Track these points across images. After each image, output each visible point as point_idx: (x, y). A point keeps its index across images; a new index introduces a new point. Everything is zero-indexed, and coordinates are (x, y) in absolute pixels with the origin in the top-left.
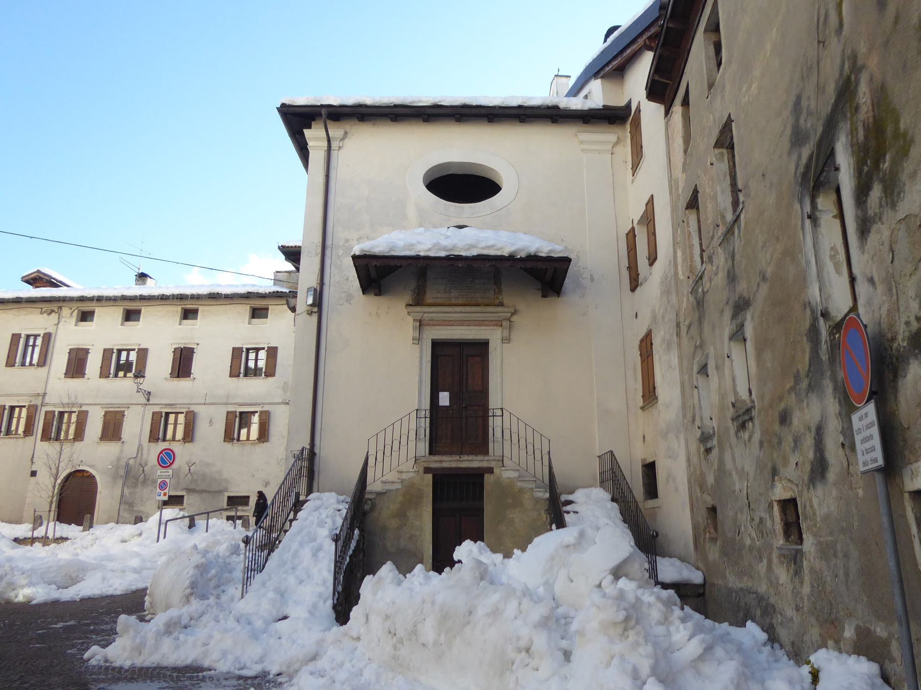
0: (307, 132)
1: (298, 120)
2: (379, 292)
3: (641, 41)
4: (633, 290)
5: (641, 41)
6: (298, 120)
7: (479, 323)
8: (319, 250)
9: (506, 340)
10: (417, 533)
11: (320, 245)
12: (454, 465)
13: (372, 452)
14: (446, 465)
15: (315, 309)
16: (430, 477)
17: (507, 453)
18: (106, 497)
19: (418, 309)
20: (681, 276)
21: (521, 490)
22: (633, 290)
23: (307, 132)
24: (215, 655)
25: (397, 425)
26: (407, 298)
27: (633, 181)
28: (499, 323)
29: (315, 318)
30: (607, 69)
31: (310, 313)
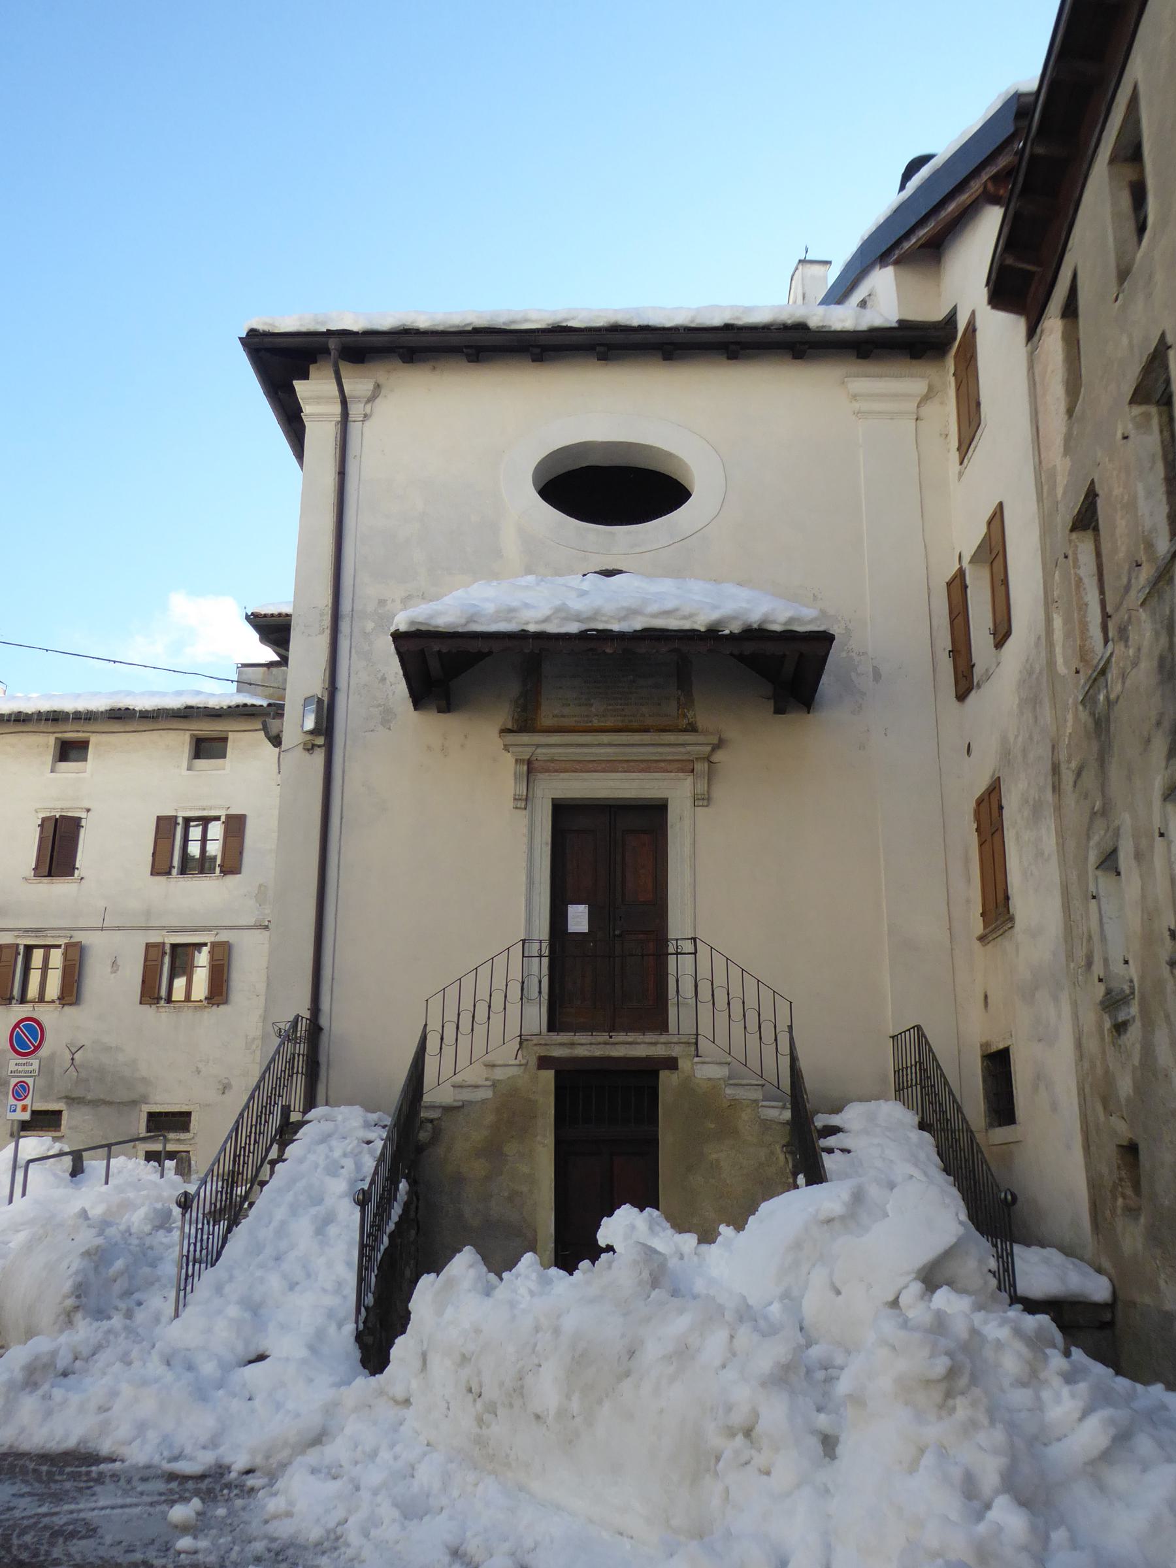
1: (281, 360)
2: (447, 705)
3: (976, 186)
5: (976, 186)
6: (281, 360)
7: (647, 766)
8: (327, 621)
9: (702, 800)
12: (598, 1052)
13: (434, 1026)
14: (581, 1052)
15: (320, 740)
16: (549, 1075)
18: (379, 676)
19: (525, 738)
23: (301, 388)
26: (504, 716)
28: (687, 767)
29: (319, 757)
31: (310, 748)
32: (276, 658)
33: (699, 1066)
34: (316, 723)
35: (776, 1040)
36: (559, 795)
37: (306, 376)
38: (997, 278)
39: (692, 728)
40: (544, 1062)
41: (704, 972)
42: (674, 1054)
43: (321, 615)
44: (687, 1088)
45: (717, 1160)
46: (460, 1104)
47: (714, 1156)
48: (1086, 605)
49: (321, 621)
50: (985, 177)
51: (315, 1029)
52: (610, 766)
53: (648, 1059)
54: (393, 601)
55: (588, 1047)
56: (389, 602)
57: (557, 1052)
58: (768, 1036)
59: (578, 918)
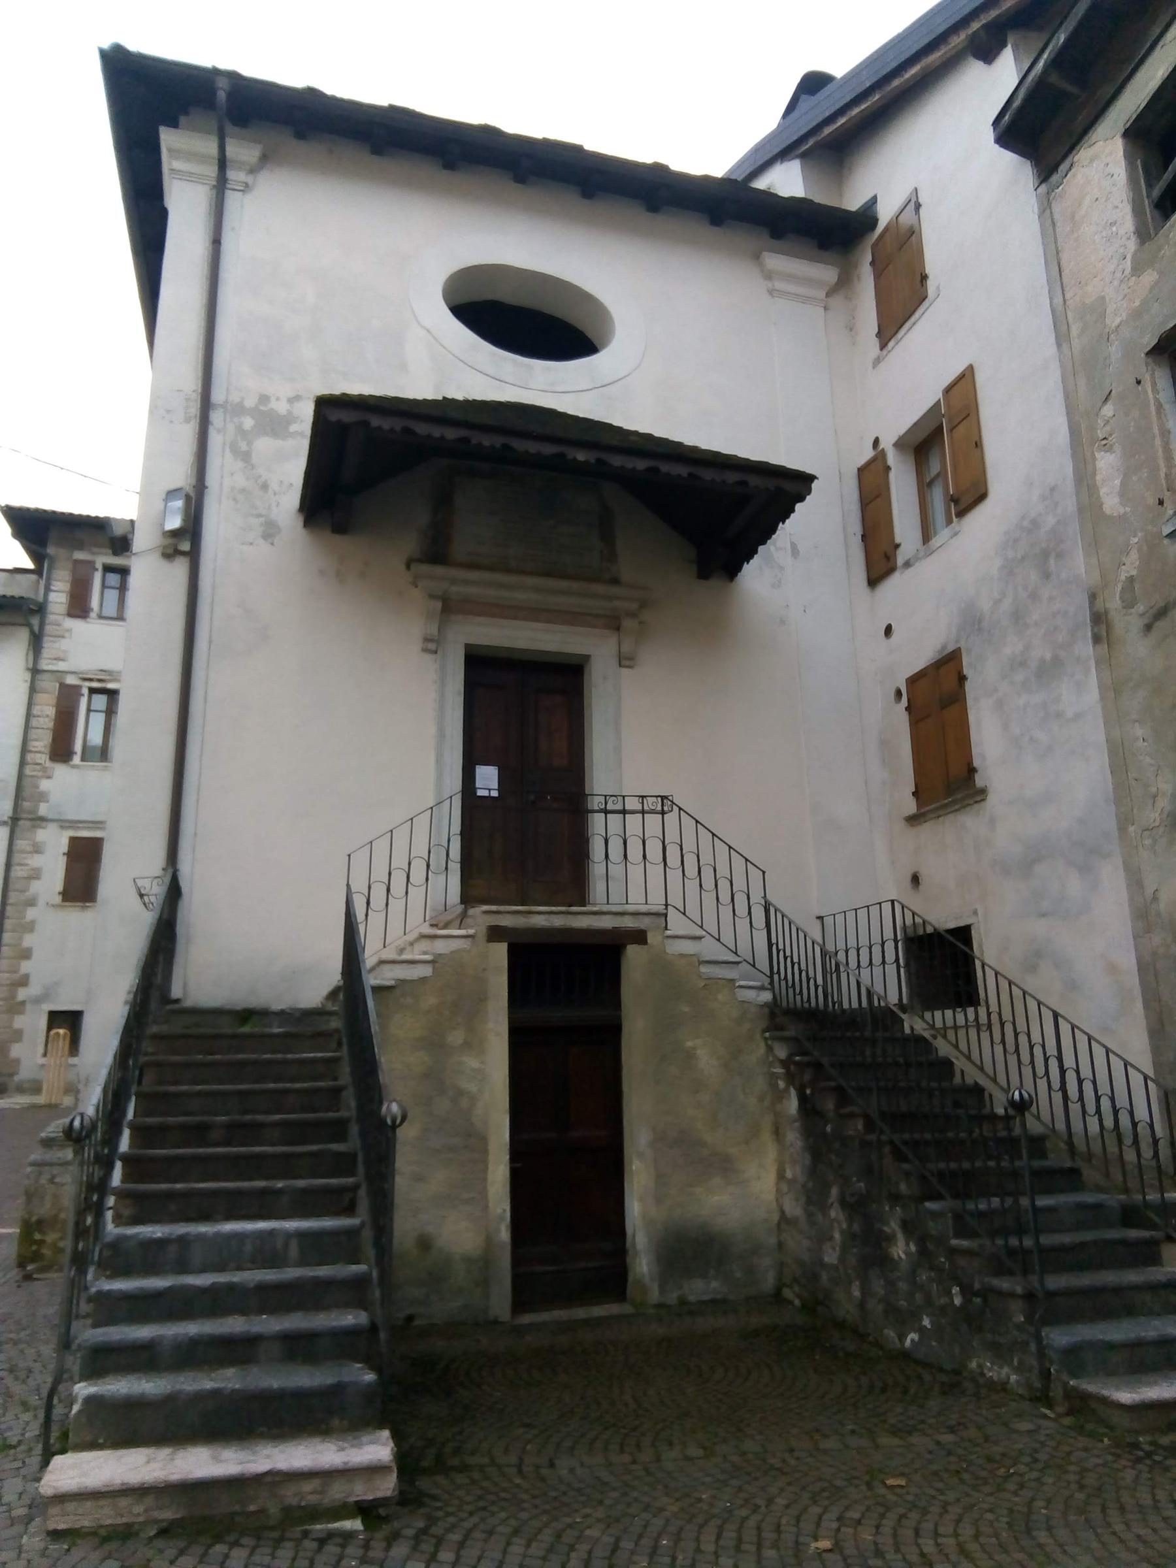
0: (168, 138)
1: (151, 100)
2: (340, 528)
3: (959, 40)
4: (874, 581)
5: (959, 40)
6: (151, 100)
7: (573, 618)
8: (195, 409)
9: (625, 660)
10: (473, 1088)
11: (196, 398)
12: (558, 922)
13: (359, 885)
14: (539, 921)
15: (186, 546)
16: (500, 952)
17: (675, 899)
18: (260, 482)
19: (439, 570)
20: (1111, 502)
21: (712, 983)
22: (874, 581)
23: (168, 138)
24: (39, 1402)
25: (382, 847)
26: (410, 544)
27: (877, 361)
28: (613, 623)
29: (180, 569)
30: (811, 142)
31: (170, 554)
32: (29, 564)
33: (670, 941)
34: (185, 520)
35: (750, 913)
36: (473, 640)
37: (174, 124)
38: (1021, 109)
39: (615, 581)
40: (495, 934)
41: (672, 836)
42: (642, 927)
43: (187, 400)
44: (662, 966)
45: (694, 1048)
46: (392, 983)
47: (689, 1044)
48: (1169, 432)
49: (187, 407)
50: (975, 26)
51: (174, 892)
52: (534, 613)
53: (615, 931)
54: (278, 399)
55: (546, 916)
56: (273, 399)
57: (507, 921)
58: (742, 909)
59: (488, 779)
